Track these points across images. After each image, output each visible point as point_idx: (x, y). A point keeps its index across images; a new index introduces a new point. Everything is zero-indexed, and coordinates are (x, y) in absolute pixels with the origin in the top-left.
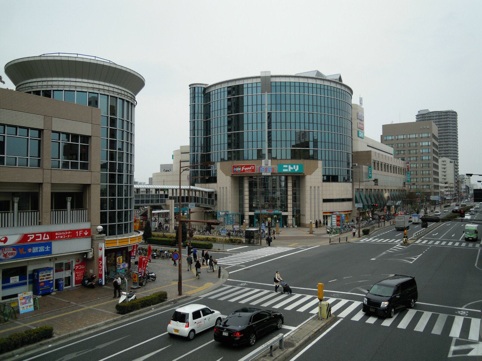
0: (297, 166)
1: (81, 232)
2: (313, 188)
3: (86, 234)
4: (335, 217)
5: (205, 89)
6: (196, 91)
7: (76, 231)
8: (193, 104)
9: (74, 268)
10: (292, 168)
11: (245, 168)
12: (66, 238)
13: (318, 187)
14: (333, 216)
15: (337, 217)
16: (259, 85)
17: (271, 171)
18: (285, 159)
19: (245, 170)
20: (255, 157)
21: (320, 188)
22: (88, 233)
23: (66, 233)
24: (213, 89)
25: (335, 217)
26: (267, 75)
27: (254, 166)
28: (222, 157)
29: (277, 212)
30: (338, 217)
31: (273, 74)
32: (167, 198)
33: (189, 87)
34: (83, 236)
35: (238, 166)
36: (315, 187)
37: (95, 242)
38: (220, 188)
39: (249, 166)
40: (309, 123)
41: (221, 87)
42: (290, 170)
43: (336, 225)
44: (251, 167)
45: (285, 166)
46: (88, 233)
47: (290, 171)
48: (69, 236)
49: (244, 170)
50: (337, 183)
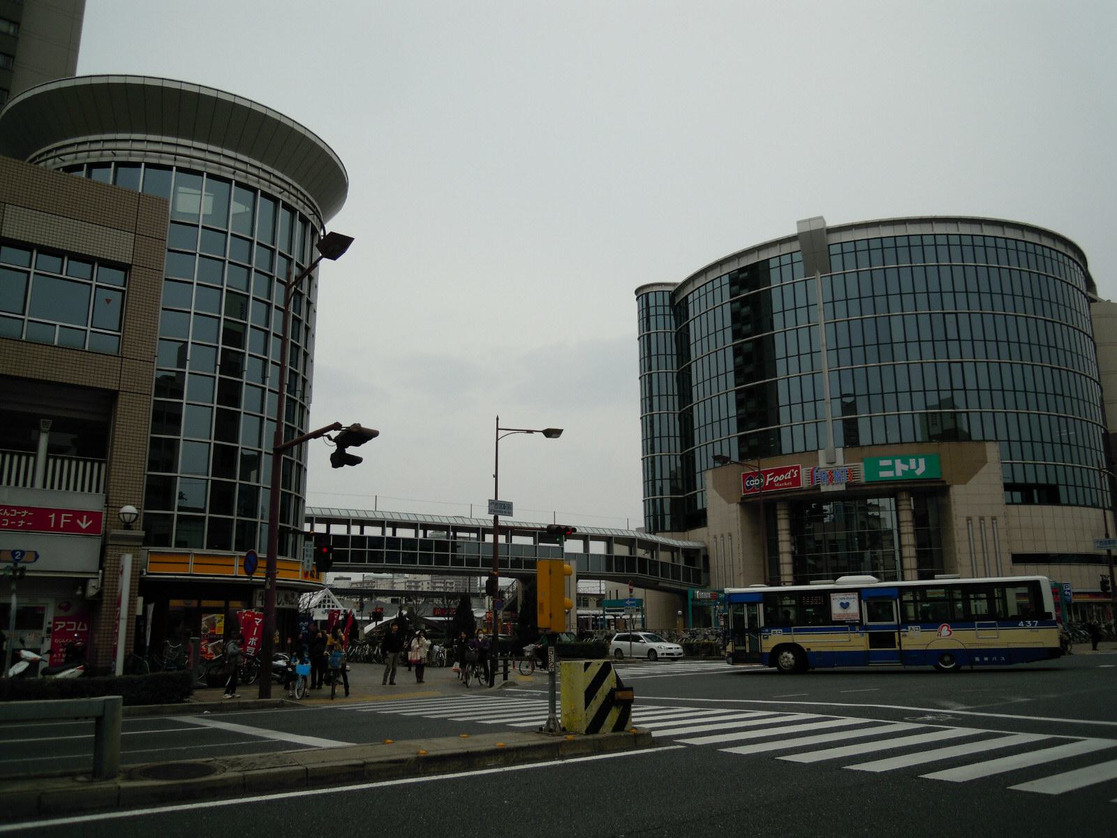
0: (922, 461)
1: (66, 518)
3: (84, 526)
5: (673, 295)
6: (652, 303)
7: (50, 511)
8: (645, 333)
9: (51, 626)
10: (906, 468)
11: (774, 476)
12: (15, 527)
13: (994, 518)
16: (797, 257)
17: (845, 479)
19: (775, 481)
21: (1001, 522)
22: (91, 522)
23: (13, 513)
24: (690, 288)
26: (814, 227)
27: (797, 468)
28: (718, 453)
31: (831, 222)
33: (636, 297)
34: (72, 528)
36: (982, 519)
37: (110, 552)
38: (715, 537)
39: (784, 471)
40: (947, 340)
42: (899, 473)
44: (790, 473)
45: (883, 463)
46: (91, 522)
47: (901, 475)
48: (22, 522)
49: (771, 482)
50: (1057, 509)
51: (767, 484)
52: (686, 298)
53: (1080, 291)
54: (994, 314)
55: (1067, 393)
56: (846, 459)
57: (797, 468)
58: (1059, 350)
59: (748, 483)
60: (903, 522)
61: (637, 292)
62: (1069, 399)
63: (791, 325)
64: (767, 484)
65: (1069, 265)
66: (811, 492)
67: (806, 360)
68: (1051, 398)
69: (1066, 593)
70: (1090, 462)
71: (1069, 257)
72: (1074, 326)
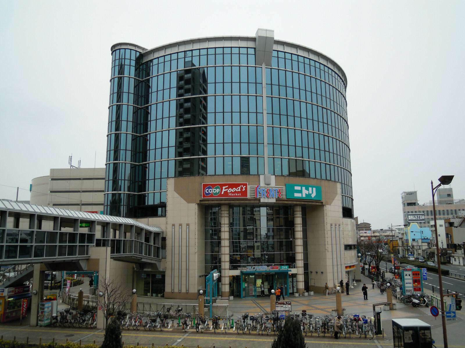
0: (314, 189)
2: (333, 226)
4: (409, 275)
5: (142, 56)
11: (228, 188)
14: (405, 274)
15: (413, 274)
18: (231, 175)
19: (228, 191)
20: (237, 169)
24: (156, 55)
25: (406, 275)
27: (246, 185)
29: (285, 268)
30: (416, 274)
31: (277, 38)
32: (92, 243)
35: (213, 186)
39: (236, 186)
41: (165, 53)
42: (304, 196)
43: (412, 289)
44: (240, 188)
45: (297, 188)
47: (305, 196)
51: (223, 193)
52: (151, 61)
53: (343, 95)
54: (287, 99)
55: (331, 151)
56: (277, 183)
57: (246, 185)
58: (329, 126)
59: (208, 191)
60: (227, 217)
61: (114, 48)
62: (339, 156)
63: (219, 92)
64: (223, 193)
65: (335, 77)
66: (252, 202)
67: (253, 116)
68: (322, 153)
69: (424, 274)
70: (346, 193)
71: (335, 73)
72: (335, 111)
